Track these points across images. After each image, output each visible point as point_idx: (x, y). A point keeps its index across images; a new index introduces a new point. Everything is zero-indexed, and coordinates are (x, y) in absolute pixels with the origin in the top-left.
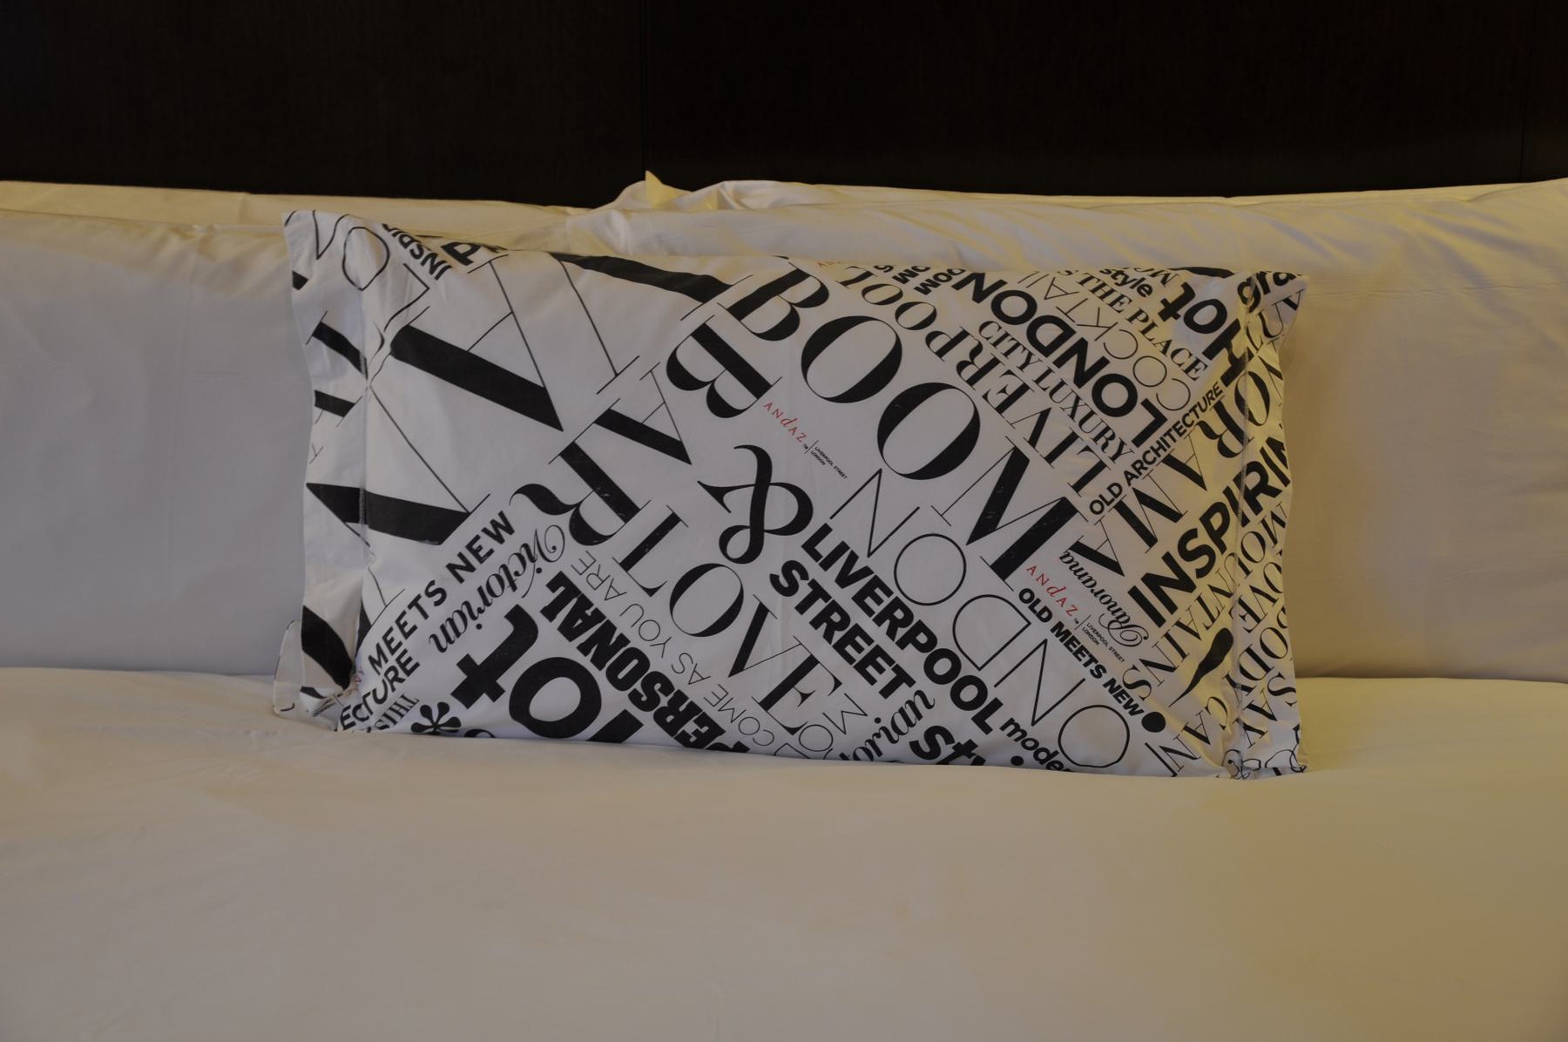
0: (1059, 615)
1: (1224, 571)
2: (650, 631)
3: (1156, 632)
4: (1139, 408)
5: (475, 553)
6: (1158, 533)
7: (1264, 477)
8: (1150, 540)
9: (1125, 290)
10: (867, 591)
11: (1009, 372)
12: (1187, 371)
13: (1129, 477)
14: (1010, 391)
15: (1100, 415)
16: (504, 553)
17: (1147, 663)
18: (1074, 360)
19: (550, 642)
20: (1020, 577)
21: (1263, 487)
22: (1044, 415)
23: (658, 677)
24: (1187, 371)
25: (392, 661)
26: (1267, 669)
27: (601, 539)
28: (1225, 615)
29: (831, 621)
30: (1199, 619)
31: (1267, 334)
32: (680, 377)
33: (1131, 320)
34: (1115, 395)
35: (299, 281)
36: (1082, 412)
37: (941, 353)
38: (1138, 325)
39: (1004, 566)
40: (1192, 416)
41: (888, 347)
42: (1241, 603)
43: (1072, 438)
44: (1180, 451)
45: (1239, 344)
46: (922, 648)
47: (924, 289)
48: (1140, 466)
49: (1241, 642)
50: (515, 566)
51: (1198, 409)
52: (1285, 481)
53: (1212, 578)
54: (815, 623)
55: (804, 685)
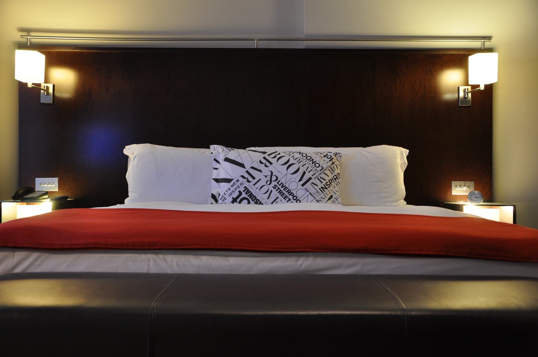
1: (331, 188)
2: (257, 193)
3: (323, 194)
4: (320, 167)
5: (234, 184)
6: (323, 182)
7: (337, 177)
8: (322, 183)
9: (319, 154)
14: (304, 164)
15: (315, 167)
16: (238, 184)
17: (321, 198)
18: (312, 161)
19: (244, 195)
20: (305, 187)
22: (308, 167)
23: (258, 199)
25: (223, 198)
26: (337, 200)
27: (250, 182)
28: (332, 193)
29: (280, 192)
30: (328, 193)
31: (337, 160)
34: (317, 165)
35: (212, 153)
36: (313, 167)
37: (295, 160)
38: (320, 158)
39: (303, 185)
41: (288, 171)
43: (312, 170)
44: (326, 172)
45: (333, 160)
46: (292, 195)
47: (293, 153)
48: (320, 174)
49: (334, 197)
50: (239, 185)
52: (340, 178)
53: (330, 188)
54: (278, 192)
55: (277, 201)
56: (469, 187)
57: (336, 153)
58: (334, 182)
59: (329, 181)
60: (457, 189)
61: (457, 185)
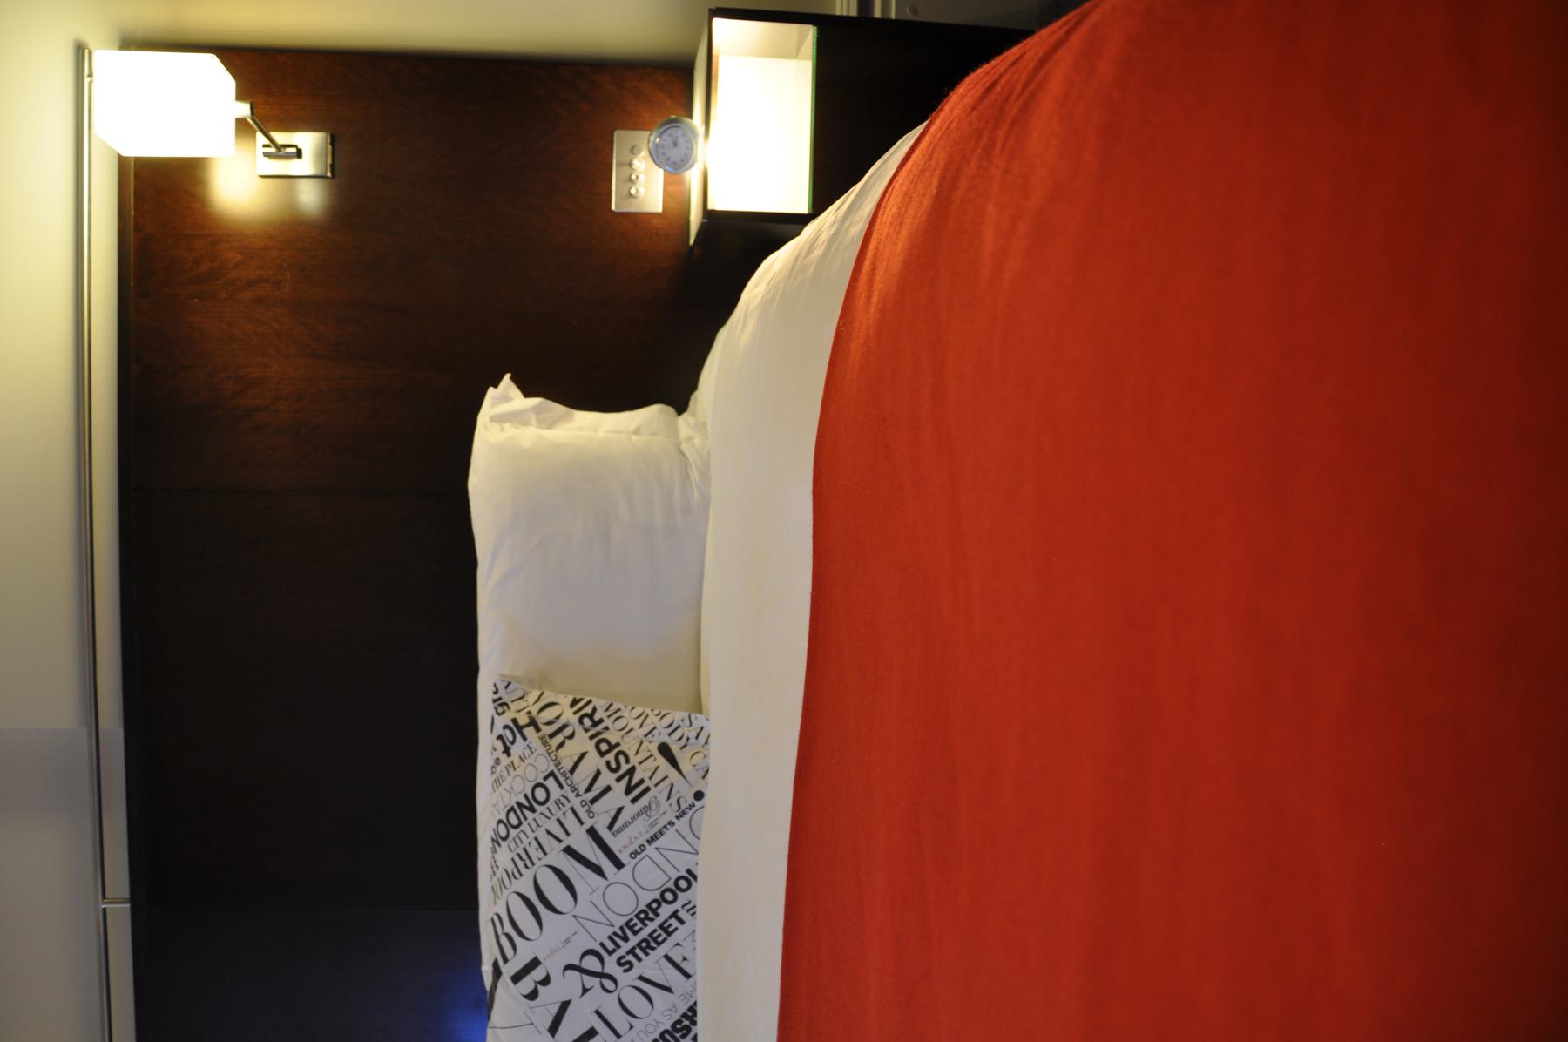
0: (643, 841)
1: (629, 746)
2: (651, 1029)
7: (586, 715)
8: (608, 789)
10: (631, 929)
11: (529, 844)
12: (532, 752)
13: (578, 795)
14: (537, 846)
15: (548, 804)
17: (669, 798)
21: (591, 716)
23: (673, 1026)
24: (532, 752)
26: (679, 727)
29: (647, 946)
32: (533, 995)
33: (509, 774)
39: (619, 865)
40: (552, 755)
42: (646, 736)
43: (559, 820)
45: (523, 720)
46: (659, 906)
48: (574, 789)
51: (550, 751)
52: (590, 702)
53: (631, 754)
54: (647, 954)
55: (678, 960)
56: (633, 151)
57: (495, 701)
58: (607, 728)
59: (602, 754)
60: (642, 191)
61: (626, 192)
